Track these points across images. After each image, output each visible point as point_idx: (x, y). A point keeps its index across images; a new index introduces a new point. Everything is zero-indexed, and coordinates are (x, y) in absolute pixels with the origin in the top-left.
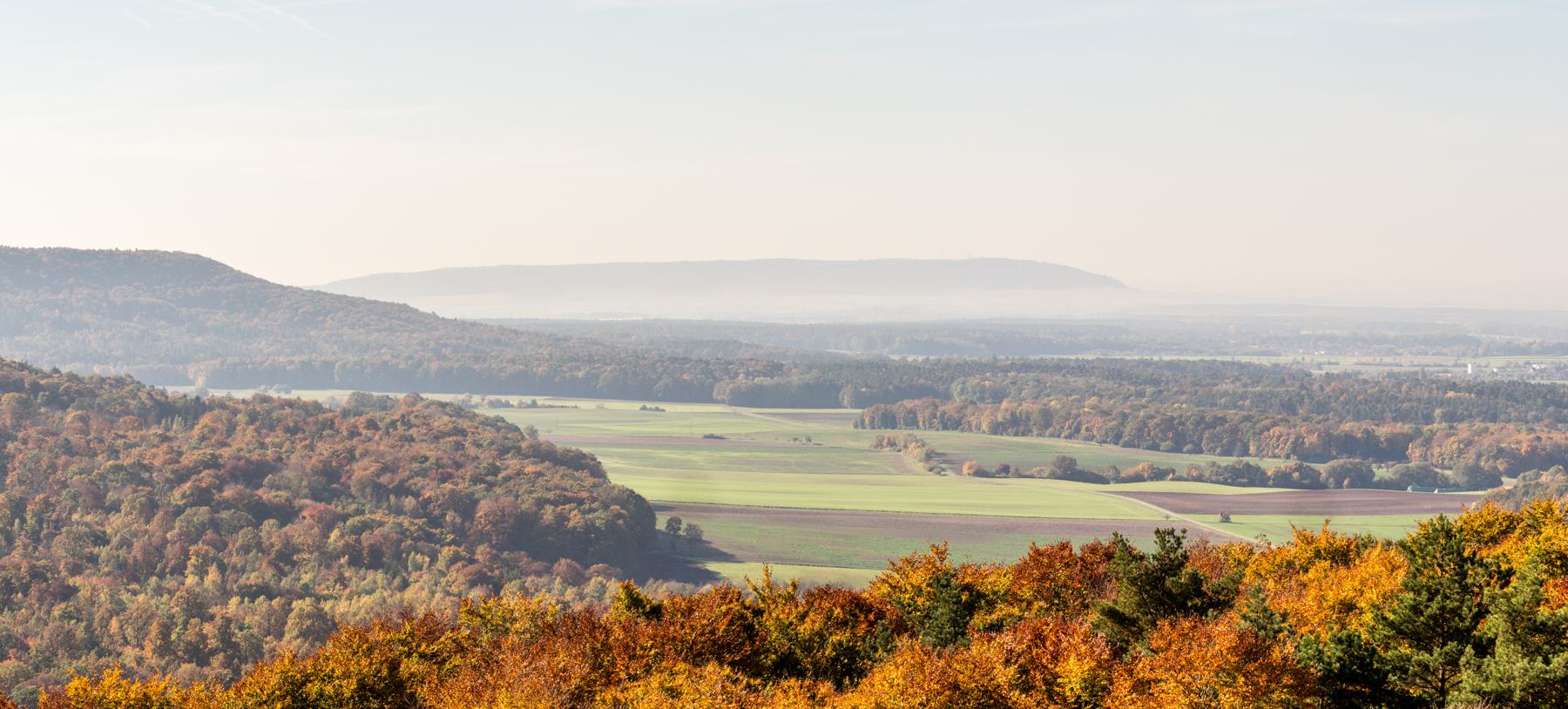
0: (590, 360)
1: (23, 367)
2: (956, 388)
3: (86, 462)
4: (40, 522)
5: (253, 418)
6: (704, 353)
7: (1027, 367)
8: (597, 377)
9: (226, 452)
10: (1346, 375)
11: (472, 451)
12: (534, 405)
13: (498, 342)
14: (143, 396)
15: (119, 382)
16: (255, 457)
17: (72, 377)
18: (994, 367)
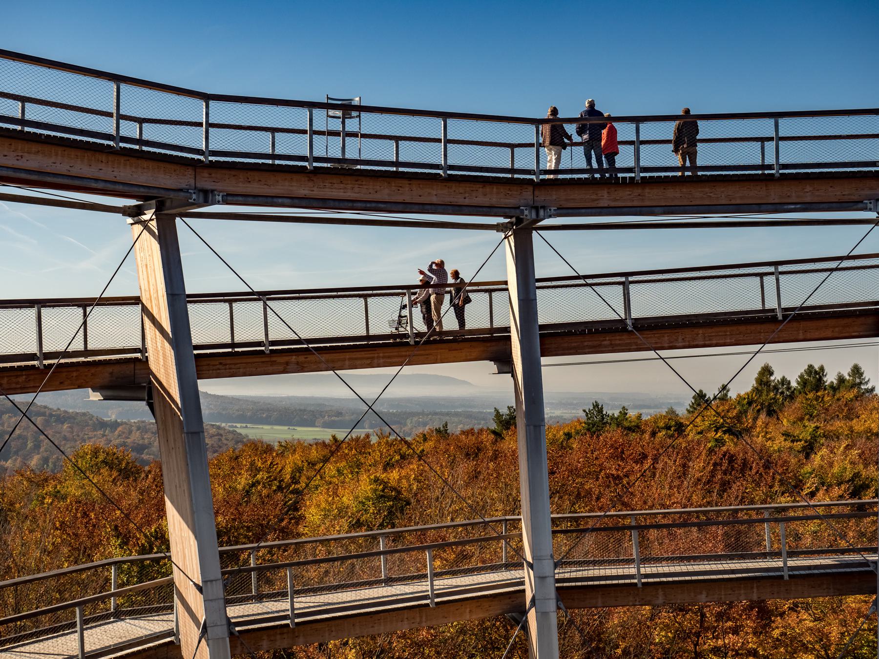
0: (268, 410)
1: (45, 407)
2: (409, 421)
3: (72, 444)
4: (55, 466)
5: (138, 428)
6: (312, 408)
7: (436, 414)
8: (270, 417)
9: (129, 441)
10: (558, 416)
11: (225, 442)
12: (246, 427)
13: (231, 403)
14: (94, 419)
15: (84, 414)
16: (141, 442)
17: (65, 412)
18: (423, 414)
